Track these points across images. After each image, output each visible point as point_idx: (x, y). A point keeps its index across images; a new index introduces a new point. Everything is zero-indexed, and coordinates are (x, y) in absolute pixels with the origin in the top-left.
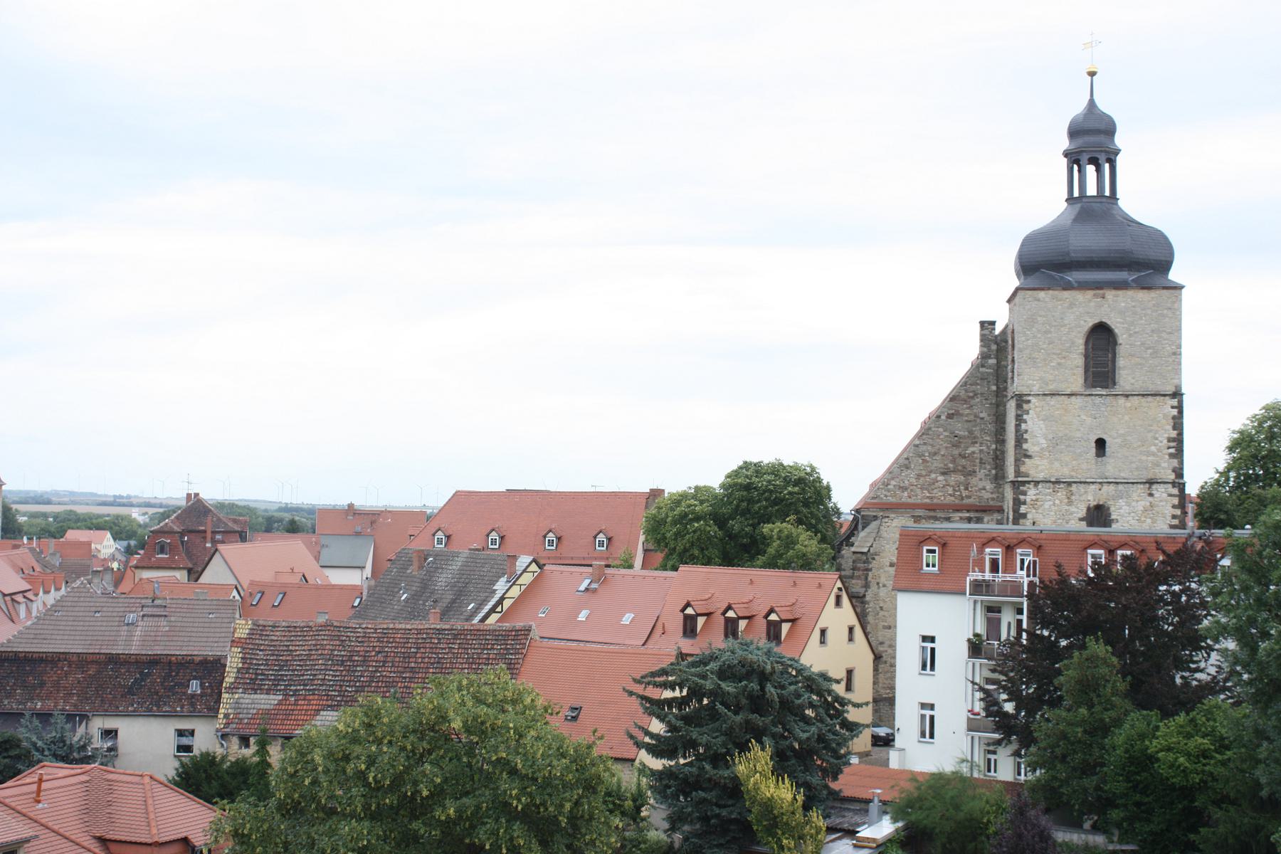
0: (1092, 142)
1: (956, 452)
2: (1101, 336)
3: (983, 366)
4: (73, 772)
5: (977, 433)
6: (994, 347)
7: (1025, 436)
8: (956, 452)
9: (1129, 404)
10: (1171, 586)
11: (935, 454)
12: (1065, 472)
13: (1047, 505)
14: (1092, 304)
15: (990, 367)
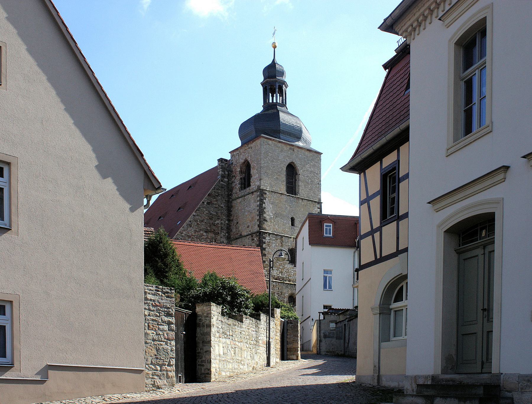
0: (273, 81)
1: (211, 222)
3: (222, 181)
5: (220, 214)
8: (211, 222)
9: (303, 203)
11: (202, 221)
13: (274, 245)
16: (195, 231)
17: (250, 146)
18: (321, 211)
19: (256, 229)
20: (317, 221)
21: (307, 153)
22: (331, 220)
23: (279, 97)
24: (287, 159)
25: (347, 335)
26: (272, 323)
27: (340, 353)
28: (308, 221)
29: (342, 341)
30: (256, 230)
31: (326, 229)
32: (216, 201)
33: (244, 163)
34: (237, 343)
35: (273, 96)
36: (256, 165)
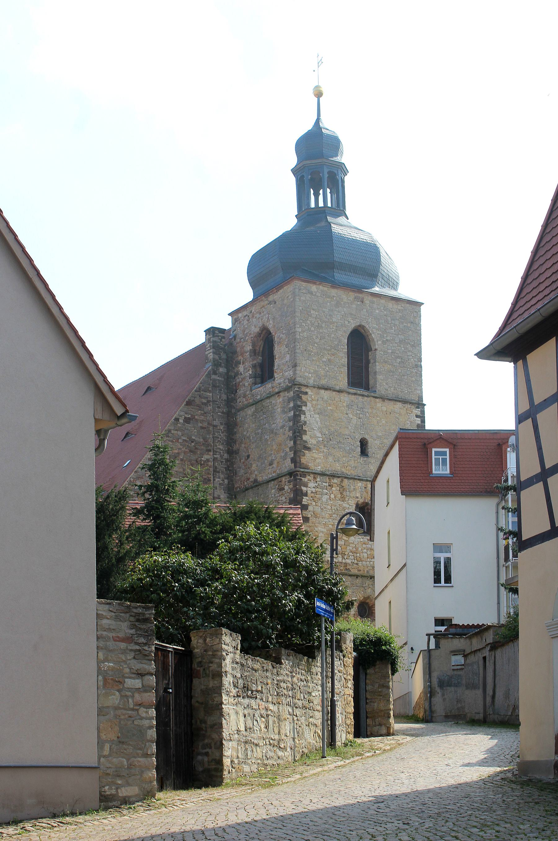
0: (318, 164)
1: (194, 457)
3: (215, 373)
4: (349, 230)
5: (211, 441)
6: (224, 356)
8: (194, 457)
12: (337, 467)
17: (271, 298)
18: (423, 421)
19: (288, 465)
20: (417, 446)
21: (391, 305)
22: (446, 441)
23: (329, 195)
24: (350, 319)
25: (490, 680)
26: (337, 663)
27: (477, 717)
28: (397, 447)
29: (480, 692)
30: (285, 470)
31: (437, 460)
32: (202, 415)
33: (259, 334)
34: (271, 707)
35: (317, 195)
36: (284, 336)
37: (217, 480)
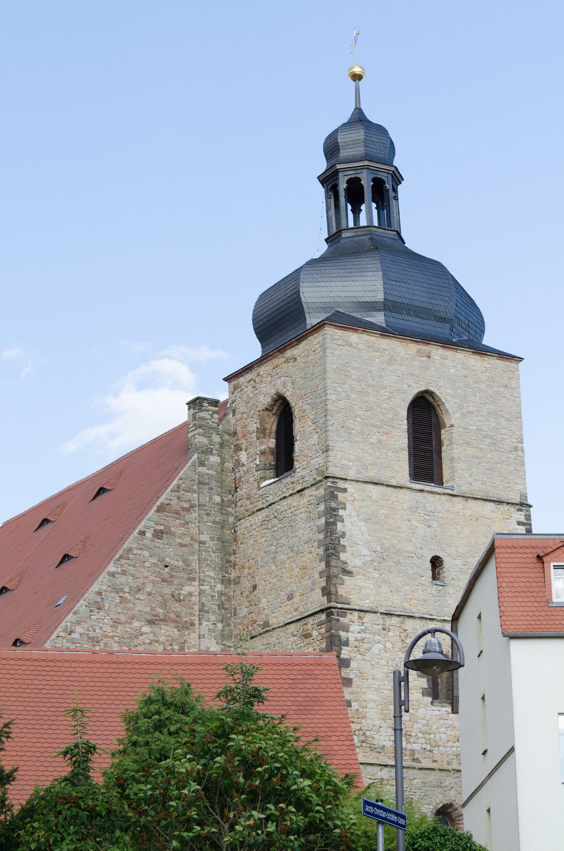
1: (167, 590)
2: (424, 414)
5: (195, 565)
7: (342, 542)
8: (167, 590)
10: (188, 836)
13: (377, 648)
14: (416, 363)
15: (211, 468)
16: (116, 622)
17: (289, 353)
19: (318, 601)
33: (275, 401)
37: (205, 623)
